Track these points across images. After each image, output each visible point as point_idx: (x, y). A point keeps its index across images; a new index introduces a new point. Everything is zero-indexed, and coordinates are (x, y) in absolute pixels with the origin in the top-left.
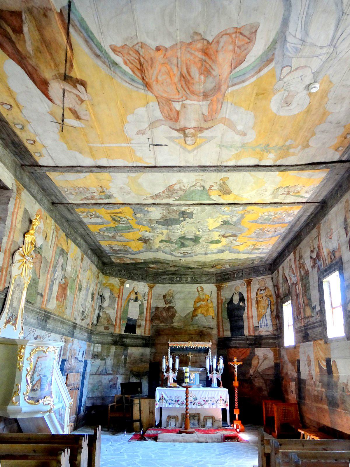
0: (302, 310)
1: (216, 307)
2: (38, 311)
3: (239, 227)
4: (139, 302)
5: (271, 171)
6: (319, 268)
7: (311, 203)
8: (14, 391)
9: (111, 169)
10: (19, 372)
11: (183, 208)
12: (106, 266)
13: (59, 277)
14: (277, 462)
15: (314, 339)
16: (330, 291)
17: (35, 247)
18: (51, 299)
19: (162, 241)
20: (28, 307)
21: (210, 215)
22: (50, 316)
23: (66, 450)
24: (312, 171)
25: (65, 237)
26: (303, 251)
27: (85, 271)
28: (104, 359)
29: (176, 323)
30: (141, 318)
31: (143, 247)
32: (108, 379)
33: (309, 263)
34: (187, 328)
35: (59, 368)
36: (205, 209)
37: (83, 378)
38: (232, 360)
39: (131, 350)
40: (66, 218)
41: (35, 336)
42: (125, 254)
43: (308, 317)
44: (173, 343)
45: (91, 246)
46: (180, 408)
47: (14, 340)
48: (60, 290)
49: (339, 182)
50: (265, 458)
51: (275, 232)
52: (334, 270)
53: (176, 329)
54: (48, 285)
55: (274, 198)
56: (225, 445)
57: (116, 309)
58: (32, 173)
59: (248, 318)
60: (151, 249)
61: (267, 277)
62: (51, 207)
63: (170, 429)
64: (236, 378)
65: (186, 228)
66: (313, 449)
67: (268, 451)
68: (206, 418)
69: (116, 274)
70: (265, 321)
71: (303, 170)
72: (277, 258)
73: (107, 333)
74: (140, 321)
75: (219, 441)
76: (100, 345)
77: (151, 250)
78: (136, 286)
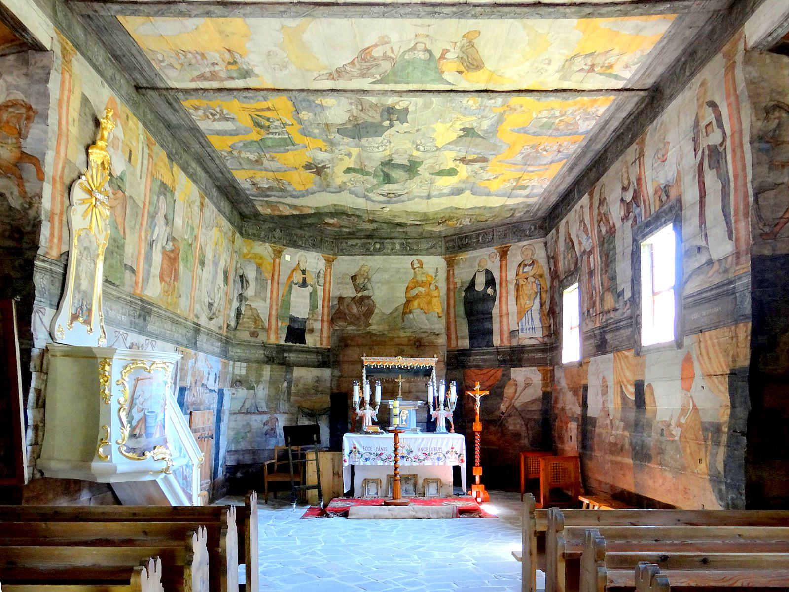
0: (598, 299)
2: (129, 299)
3: (492, 141)
5: (565, 16)
6: (635, 220)
7: (633, 90)
8: (99, 438)
9: (248, 9)
10: (105, 405)
11: (390, 101)
13: (161, 237)
14: (560, 544)
15: (617, 350)
16: (652, 263)
17: (111, 174)
18: (151, 279)
19: (348, 170)
20: (109, 290)
21: (440, 117)
22: (151, 310)
23: (200, 529)
24: (644, 17)
25: (166, 160)
26: (607, 190)
27: (209, 227)
28: (253, 388)
29: (376, 325)
30: (313, 316)
31: (314, 183)
33: (616, 212)
34: (394, 334)
35: (176, 400)
36: (432, 103)
37: (219, 419)
40: (166, 121)
41: (128, 345)
42: (281, 197)
43: (609, 312)
44: (371, 359)
45: (218, 179)
47: (89, 349)
48: (165, 262)
49: (691, 44)
50: (534, 540)
51: (559, 152)
53: (375, 335)
54: (143, 252)
55: (563, 78)
56: (459, 523)
57: (268, 301)
58: (89, 16)
59: (501, 316)
60: (328, 186)
61: (537, 243)
62: (134, 95)
63: (369, 499)
64: (478, 418)
65: (394, 143)
66: (616, 524)
67: (540, 528)
68: (427, 481)
70: (530, 320)
71: (626, 14)
72: (556, 206)
73: (254, 342)
75: (448, 516)
76: (244, 364)
77: (328, 190)
78: (303, 258)
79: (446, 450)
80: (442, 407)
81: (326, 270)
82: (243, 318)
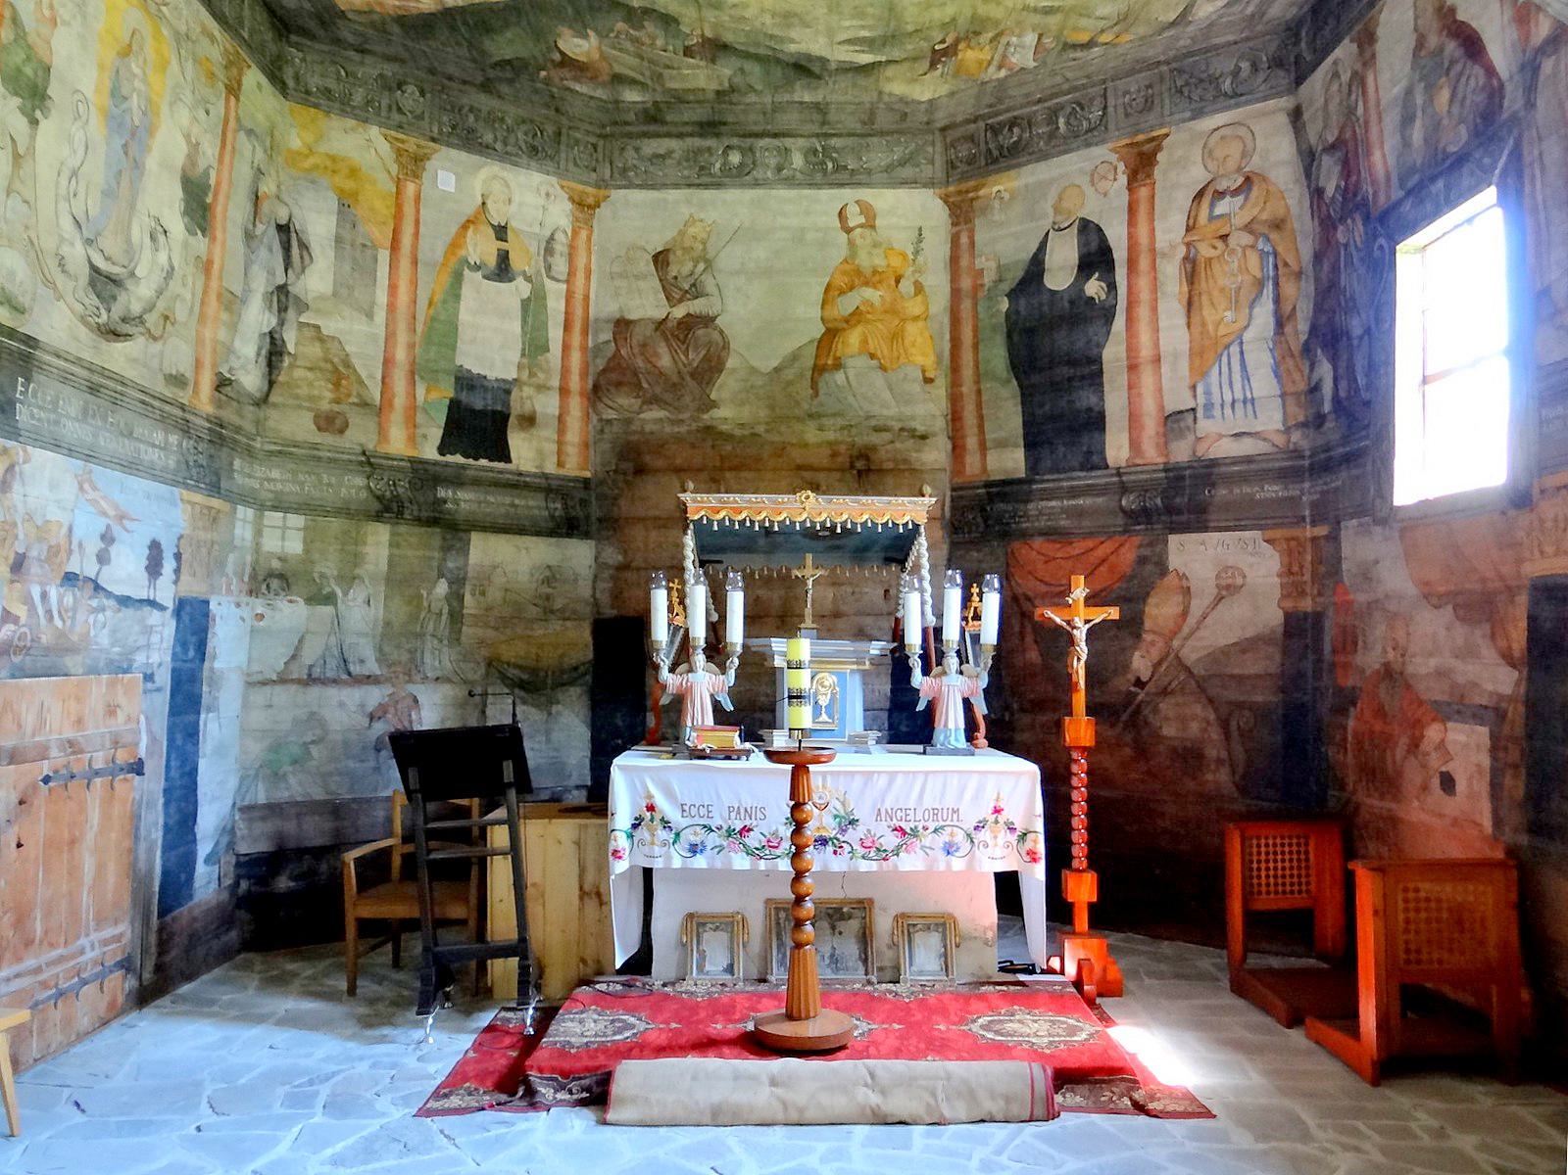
1: (946, 321)
4: (521, 288)
12: (298, 46)
28: (329, 599)
29: (731, 407)
32: (362, 706)
38: (1059, 596)
39: (484, 550)
44: (712, 499)
46: (753, 871)
53: (728, 437)
57: (380, 316)
59: (1133, 368)
61: (1264, 114)
64: (1080, 700)
68: (908, 926)
74: (527, 391)
75: (1015, 1110)
76: (296, 520)
79: (968, 816)
80: (952, 661)
81: (575, 233)
82: (292, 366)
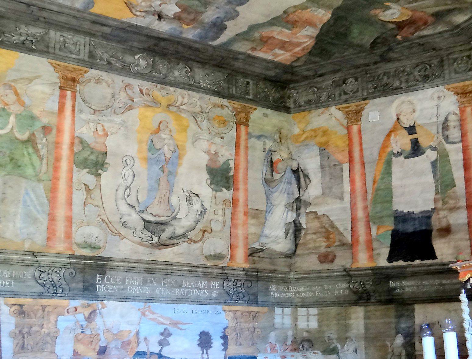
12: (293, 88)
52: (421, 343)
69: (329, 97)
73: (328, 271)
74: (442, 214)
76: (314, 311)
78: (406, 108)
